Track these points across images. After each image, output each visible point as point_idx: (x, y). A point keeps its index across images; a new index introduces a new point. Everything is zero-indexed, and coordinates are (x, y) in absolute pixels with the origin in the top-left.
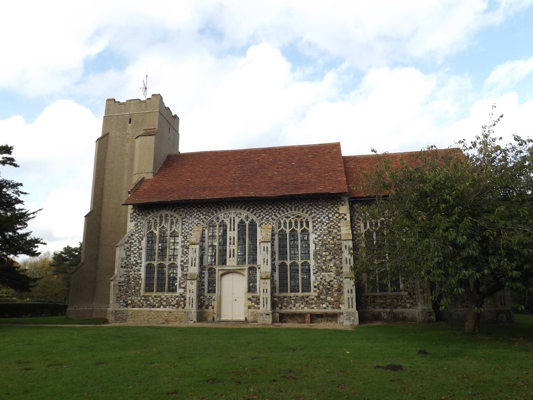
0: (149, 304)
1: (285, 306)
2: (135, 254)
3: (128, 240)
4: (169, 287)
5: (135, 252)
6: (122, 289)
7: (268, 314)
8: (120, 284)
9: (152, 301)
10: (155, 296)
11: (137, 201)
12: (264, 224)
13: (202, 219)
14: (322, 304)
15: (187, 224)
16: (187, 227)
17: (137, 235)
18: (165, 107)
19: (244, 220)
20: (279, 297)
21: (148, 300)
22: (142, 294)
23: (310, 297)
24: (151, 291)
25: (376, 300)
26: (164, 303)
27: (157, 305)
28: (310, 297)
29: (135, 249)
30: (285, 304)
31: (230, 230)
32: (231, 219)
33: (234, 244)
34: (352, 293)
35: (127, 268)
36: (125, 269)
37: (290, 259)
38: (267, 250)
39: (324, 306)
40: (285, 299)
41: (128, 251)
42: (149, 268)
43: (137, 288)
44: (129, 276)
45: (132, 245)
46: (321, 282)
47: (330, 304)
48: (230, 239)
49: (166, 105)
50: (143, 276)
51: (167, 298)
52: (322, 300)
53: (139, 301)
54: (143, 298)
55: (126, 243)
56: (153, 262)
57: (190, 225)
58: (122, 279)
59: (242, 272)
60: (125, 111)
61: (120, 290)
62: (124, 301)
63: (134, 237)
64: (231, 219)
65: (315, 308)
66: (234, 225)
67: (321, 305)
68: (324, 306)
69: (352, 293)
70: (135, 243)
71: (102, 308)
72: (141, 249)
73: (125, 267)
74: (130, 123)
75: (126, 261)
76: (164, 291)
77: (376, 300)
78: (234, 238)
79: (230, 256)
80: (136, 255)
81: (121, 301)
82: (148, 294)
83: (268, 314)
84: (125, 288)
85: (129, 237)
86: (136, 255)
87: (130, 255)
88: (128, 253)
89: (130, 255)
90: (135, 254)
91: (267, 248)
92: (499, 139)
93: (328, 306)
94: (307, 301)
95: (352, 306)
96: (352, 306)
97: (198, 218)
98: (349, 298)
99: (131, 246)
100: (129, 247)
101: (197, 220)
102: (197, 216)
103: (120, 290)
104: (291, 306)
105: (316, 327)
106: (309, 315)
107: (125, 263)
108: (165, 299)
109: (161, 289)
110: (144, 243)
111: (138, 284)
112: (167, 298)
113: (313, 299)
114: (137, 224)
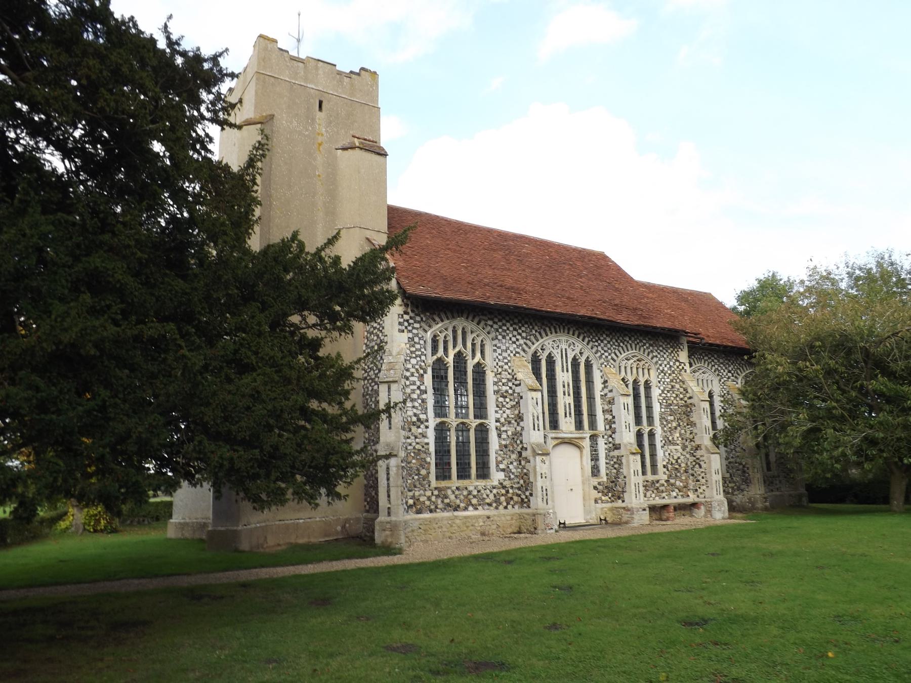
0: (448, 505)
2: (413, 400)
8: (473, 471)
15: (499, 351)
24: (468, 477)
26: (474, 501)
27: (462, 505)
39: (674, 494)
59: (557, 442)
68: (674, 494)
71: (286, 522)
82: (443, 484)
94: (657, 489)
108: (475, 493)
111: (424, 464)
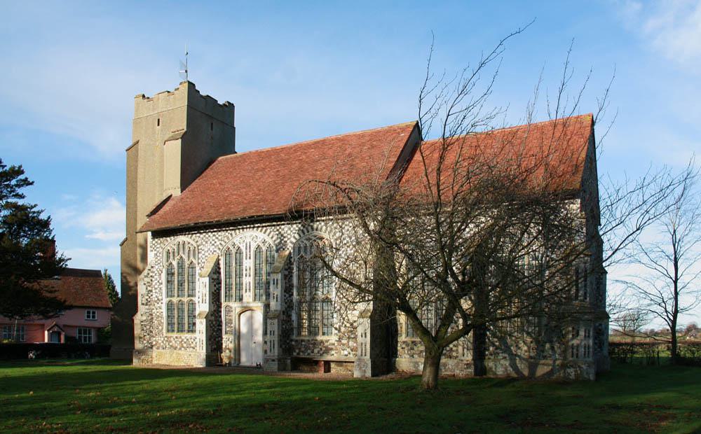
1: (303, 352)
2: (156, 289)
3: (148, 274)
4: (189, 327)
5: (156, 286)
6: (145, 329)
7: (273, 360)
9: (174, 342)
10: (177, 337)
11: (156, 227)
12: (282, 249)
13: (218, 245)
14: (344, 350)
15: (203, 252)
16: (204, 256)
17: (157, 267)
18: (202, 96)
19: (261, 245)
20: (296, 341)
21: (171, 342)
22: (165, 335)
23: (330, 342)
25: (415, 347)
26: (185, 345)
28: (330, 342)
29: (156, 284)
30: (303, 349)
31: (246, 259)
32: (246, 244)
33: (250, 276)
34: (366, 337)
35: (150, 305)
36: (147, 307)
37: (178, 296)
38: (277, 283)
40: (303, 343)
41: (149, 286)
42: (170, 306)
43: (160, 328)
44: (151, 315)
45: (153, 279)
46: (343, 323)
47: (352, 350)
48: (246, 270)
49: (203, 93)
50: (165, 315)
51: (187, 340)
52: (344, 345)
53: (163, 342)
54: (166, 339)
55: (146, 277)
56: (182, 299)
57: (207, 254)
58: (144, 318)
60: (154, 109)
61: (143, 330)
62: (148, 342)
63: (154, 270)
64: (246, 244)
65: (335, 355)
66: (250, 252)
67: (342, 352)
69: (366, 337)
70: (155, 277)
72: (162, 284)
73: (147, 305)
74: (158, 125)
75: (147, 297)
76: (173, 331)
77: (415, 347)
78: (250, 269)
79: (246, 291)
80: (157, 291)
81: (145, 342)
83: (273, 360)
84: (148, 327)
85: (149, 270)
86: (157, 291)
87: (151, 291)
88: (149, 288)
89: (151, 291)
90: (156, 289)
91: (277, 280)
92: (33, 182)
93: (349, 353)
95: (365, 353)
96: (365, 353)
97: (213, 245)
98: (362, 344)
99: (152, 280)
100: (149, 281)
101: (213, 247)
102: (213, 242)
103: (143, 330)
104: (309, 351)
105: (295, 377)
106: (323, 363)
107: (147, 300)
108: (185, 340)
109: (181, 330)
110: (164, 276)
111: (160, 324)
112: (187, 340)
113: (334, 344)
114: (156, 254)
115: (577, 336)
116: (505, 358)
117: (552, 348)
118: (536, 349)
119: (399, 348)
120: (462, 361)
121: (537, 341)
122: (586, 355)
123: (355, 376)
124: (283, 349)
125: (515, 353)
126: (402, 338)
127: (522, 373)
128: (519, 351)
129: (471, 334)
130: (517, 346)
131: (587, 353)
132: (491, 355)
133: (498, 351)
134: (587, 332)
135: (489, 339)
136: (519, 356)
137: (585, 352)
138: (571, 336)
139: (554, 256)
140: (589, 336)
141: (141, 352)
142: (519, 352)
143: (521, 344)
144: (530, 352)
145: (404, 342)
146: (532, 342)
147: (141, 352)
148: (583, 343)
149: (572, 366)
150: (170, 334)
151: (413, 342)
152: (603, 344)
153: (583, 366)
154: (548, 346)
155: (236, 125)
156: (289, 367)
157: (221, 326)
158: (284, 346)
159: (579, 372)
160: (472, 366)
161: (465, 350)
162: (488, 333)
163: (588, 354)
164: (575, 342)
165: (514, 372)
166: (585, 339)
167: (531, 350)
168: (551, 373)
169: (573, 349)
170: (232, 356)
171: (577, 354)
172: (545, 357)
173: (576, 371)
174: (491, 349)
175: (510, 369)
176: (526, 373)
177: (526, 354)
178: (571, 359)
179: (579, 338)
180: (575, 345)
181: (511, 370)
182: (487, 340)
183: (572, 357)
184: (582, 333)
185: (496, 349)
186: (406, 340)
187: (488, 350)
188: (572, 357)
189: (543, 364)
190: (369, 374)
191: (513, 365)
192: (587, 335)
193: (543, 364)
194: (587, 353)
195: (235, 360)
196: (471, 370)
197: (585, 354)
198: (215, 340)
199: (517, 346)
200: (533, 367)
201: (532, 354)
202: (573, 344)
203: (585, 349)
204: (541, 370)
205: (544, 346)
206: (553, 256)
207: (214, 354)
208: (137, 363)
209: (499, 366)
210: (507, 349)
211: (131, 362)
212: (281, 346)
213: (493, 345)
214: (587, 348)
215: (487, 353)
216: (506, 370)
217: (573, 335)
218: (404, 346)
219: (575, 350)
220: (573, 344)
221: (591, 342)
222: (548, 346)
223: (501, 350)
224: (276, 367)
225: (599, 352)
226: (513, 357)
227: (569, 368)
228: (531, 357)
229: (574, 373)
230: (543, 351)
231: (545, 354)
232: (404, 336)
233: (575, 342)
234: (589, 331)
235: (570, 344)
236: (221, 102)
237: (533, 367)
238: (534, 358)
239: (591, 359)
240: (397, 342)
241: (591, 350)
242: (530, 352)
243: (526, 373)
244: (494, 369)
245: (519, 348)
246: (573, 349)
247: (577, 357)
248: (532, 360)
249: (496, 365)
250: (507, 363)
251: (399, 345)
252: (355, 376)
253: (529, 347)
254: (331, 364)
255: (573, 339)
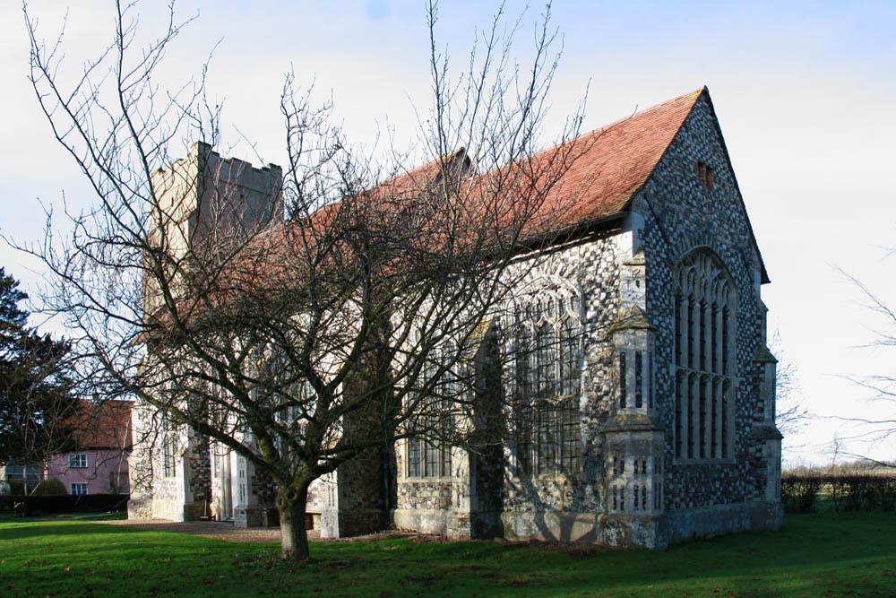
7: (242, 513)
115: (622, 473)
116: (529, 509)
117: (596, 493)
118: (572, 495)
119: (399, 494)
120: (456, 513)
121: (575, 483)
122: (640, 506)
123: (322, 536)
124: (260, 496)
125: (543, 502)
126: (402, 479)
127: (550, 534)
128: (549, 498)
129: (325, 461)
130: (545, 490)
131: (640, 501)
132: (512, 504)
133: (520, 498)
134: (640, 464)
135: (508, 480)
136: (549, 507)
137: (636, 500)
138: (612, 473)
139: (594, 335)
140: (644, 472)
141: (138, 503)
142: (549, 500)
143: (551, 488)
144: (563, 500)
145: (405, 485)
146: (566, 484)
147: (138, 503)
148: (632, 485)
149: (613, 525)
150: (167, 479)
151: (415, 485)
152: (765, 484)
153: (630, 524)
154: (589, 489)
155: (773, 345)
156: (266, 522)
157: (210, 466)
158: (261, 493)
159: (623, 534)
160: (469, 523)
161: (461, 497)
162: (506, 469)
163: (644, 503)
164: (619, 482)
165: (540, 533)
166: (636, 478)
167: (565, 498)
168: (591, 535)
169: (615, 494)
170: (221, 506)
171: (622, 503)
172: (585, 509)
173: (619, 534)
174: (511, 494)
175: (534, 527)
176: (557, 534)
177: (559, 503)
178: (613, 512)
179: (624, 475)
180: (619, 487)
181: (537, 529)
182: (505, 481)
183: (615, 508)
184: (629, 466)
185: (518, 495)
186: (407, 481)
187: (507, 496)
188: (615, 508)
189: (581, 520)
190: (336, 533)
191: (540, 522)
192: (640, 469)
193: (581, 520)
194: (640, 501)
195: (225, 512)
196: (467, 529)
197: (636, 505)
198: (201, 485)
199: (545, 490)
200: (566, 525)
201: (566, 504)
202: (615, 486)
203: (636, 495)
204: (579, 531)
205: (583, 490)
206: (526, 323)
207: (198, 504)
208: (133, 517)
209: (519, 523)
210: (532, 496)
211: (126, 517)
212: (255, 492)
213: (515, 489)
214: (640, 494)
215: (505, 501)
216: (530, 530)
217: (615, 470)
218: (404, 491)
219: (618, 497)
220: (615, 486)
221: (649, 483)
222: (589, 489)
223: (525, 496)
224: (245, 521)
225: (757, 496)
226: (541, 507)
227: (608, 528)
228: (565, 509)
229: (615, 536)
230: (582, 499)
231: (586, 502)
232: (404, 476)
233: (619, 482)
234: (644, 463)
235: (611, 485)
236: (257, 165)
237: (566, 525)
238: (570, 510)
239: (650, 512)
240: (396, 485)
241: (649, 497)
242: (563, 500)
243: (557, 534)
244: (513, 528)
245: (549, 493)
246: (615, 494)
247: (622, 508)
248: (567, 513)
249: (516, 521)
250: (532, 518)
251: (399, 489)
252: (322, 536)
253: (562, 493)
254: (314, 517)
255: (614, 477)
